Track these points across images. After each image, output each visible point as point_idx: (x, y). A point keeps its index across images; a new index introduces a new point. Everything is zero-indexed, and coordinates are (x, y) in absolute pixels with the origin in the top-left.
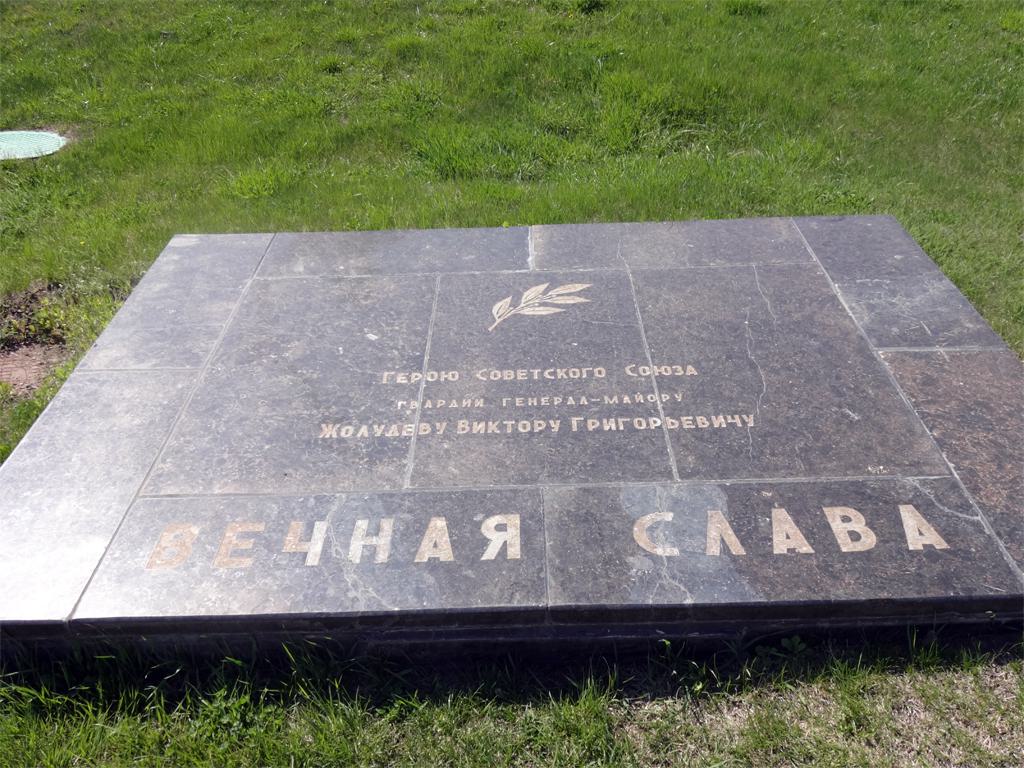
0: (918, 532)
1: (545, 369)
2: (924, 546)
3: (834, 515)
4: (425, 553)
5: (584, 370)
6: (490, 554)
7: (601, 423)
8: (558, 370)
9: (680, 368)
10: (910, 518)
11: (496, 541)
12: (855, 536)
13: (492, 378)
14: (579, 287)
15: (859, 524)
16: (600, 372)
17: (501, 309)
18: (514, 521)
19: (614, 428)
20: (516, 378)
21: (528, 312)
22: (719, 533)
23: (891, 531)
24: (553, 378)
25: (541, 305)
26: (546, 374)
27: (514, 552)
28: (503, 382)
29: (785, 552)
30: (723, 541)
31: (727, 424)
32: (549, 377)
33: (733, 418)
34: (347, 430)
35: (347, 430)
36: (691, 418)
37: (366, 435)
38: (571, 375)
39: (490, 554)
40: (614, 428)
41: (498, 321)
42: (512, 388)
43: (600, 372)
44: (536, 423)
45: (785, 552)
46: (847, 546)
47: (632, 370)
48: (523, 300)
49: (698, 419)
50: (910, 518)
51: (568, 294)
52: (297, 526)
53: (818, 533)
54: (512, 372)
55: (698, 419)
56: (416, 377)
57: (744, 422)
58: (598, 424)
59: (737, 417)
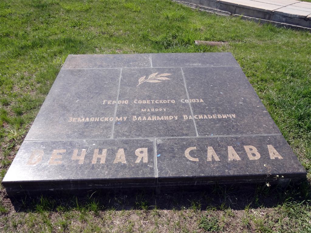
0: (273, 153)
1: (155, 100)
2: (275, 158)
3: (246, 148)
4: (115, 162)
5: (168, 101)
6: (138, 161)
7: (222, 117)
8: (160, 101)
9: (198, 100)
10: (271, 149)
11: (140, 156)
12: (254, 155)
13: (139, 103)
14: (169, 74)
15: (255, 150)
16: (173, 102)
17: (141, 80)
18: (145, 150)
19: (168, 119)
20: (142, 103)
21: (151, 81)
22: (121, 156)
23: (264, 152)
24: (158, 103)
25: (154, 79)
26: (156, 102)
27: (146, 160)
28: (142, 104)
29: (274, 159)
30: (213, 157)
31: (227, 117)
32: (157, 103)
33: (229, 115)
34: (112, 119)
35: (112, 119)
36: (197, 115)
37: (121, 120)
38: (164, 102)
39: (138, 161)
40: (163, 119)
41: (140, 83)
42: (144, 106)
43: (173, 102)
44: (160, 109)
45: (274, 159)
46: (251, 158)
47: (136, 102)
48: (149, 77)
49: (218, 115)
50: (271, 149)
51: (164, 77)
52: (76, 151)
53: (264, 152)
54: (145, 101)
55: (218, 115)
56: (114, 102)
57: (208, 117)
58: (212, 117)
59: (230, 115)
